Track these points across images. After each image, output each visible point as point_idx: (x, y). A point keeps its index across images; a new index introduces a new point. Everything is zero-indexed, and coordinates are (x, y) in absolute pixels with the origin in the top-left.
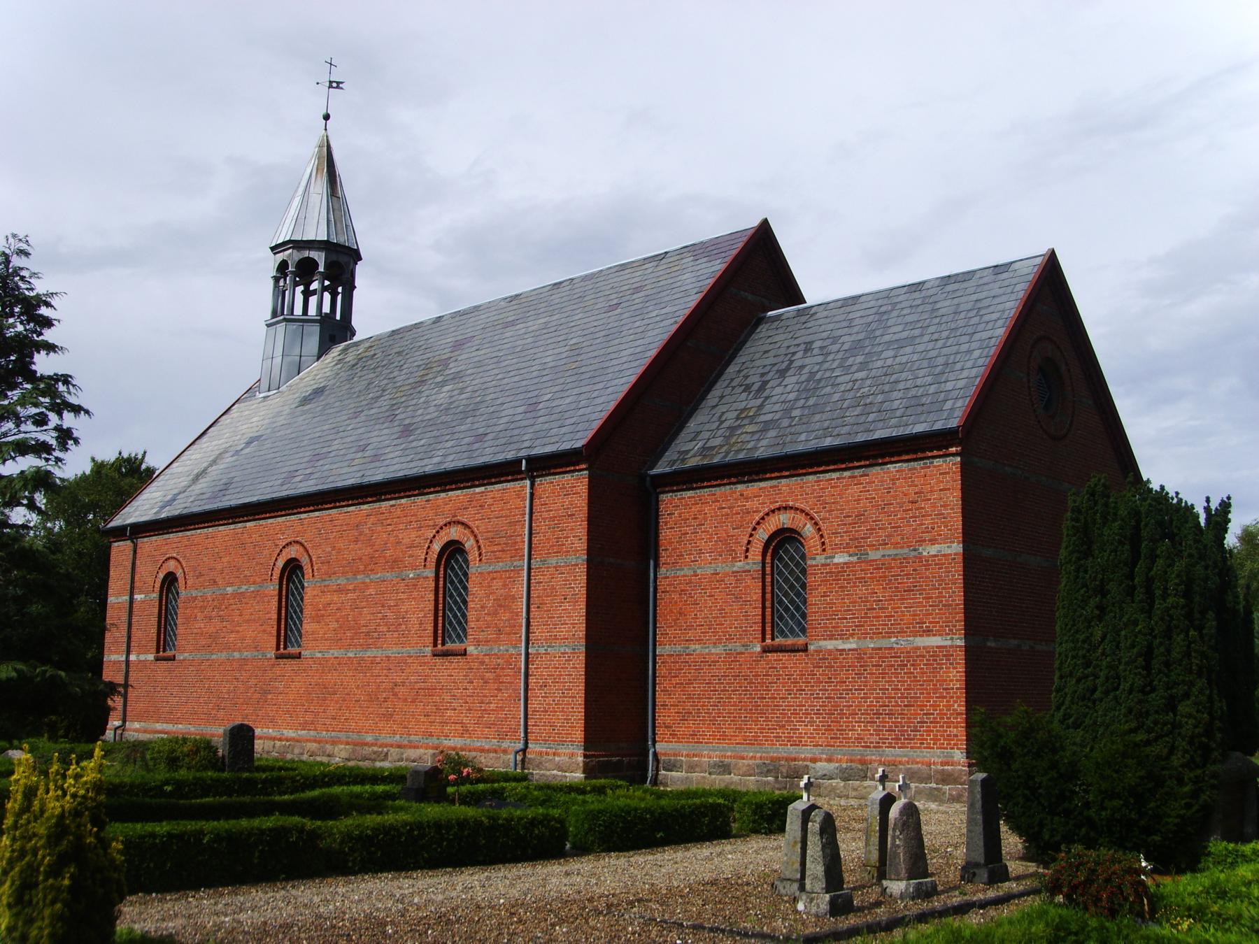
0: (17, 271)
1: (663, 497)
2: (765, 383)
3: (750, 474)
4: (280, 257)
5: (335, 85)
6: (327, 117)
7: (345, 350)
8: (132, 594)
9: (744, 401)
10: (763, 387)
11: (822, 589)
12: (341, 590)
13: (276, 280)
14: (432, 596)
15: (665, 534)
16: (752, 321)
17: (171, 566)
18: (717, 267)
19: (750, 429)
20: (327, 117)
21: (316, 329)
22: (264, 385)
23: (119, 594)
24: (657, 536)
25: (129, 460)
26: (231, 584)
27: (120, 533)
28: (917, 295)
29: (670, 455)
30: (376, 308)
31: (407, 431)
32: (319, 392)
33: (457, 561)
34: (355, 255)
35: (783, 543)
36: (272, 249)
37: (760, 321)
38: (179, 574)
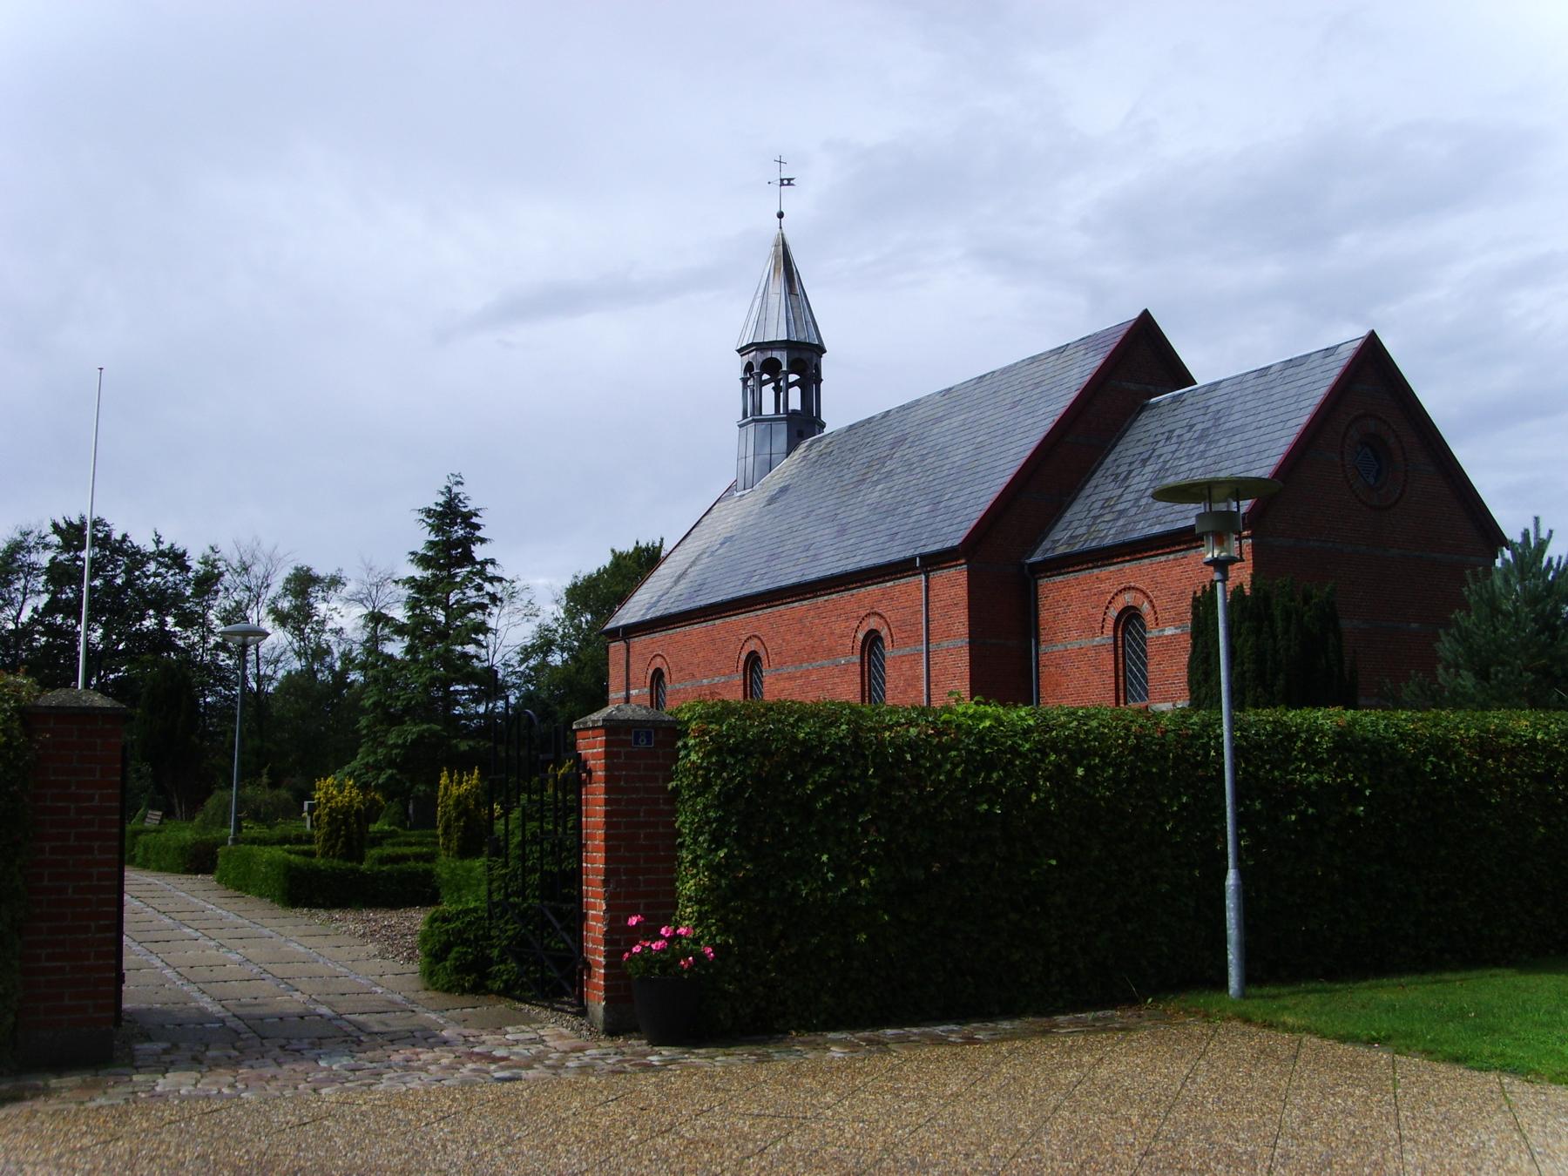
0: (457, 495)
1: (1040, 582)
2: (1130, 472)
3: (1102, 559)
4: (746, 359)
5: (787, 182)
6: (781, 215)
7: (811, 445)
8: (628, 690)
9: (1111, 490)
10: (1126, 478)
11: (1157, 659)
12: (791, 678)
13: (745, 381)
14: (859, 680)
15: (1044, 615)
16: (1136, 407)
17: (658, 662)
18: (1095, 361)
19: (1107, 518)
20: (781, 215)
21: (783, 427)
22: (740, 485)
23: (618, 690)
24: (1037, 616)
25: (647, 549)
26: (706, 677)
27: (614, 634)
28: (1262, 380)
29: (1046, 544)
30: (844, 400)
31: (842, 531)
32: (784, 490)
33: (1134, 626)
34: (820, 350)
35: (1129, 619)
36: (739, 351)
37: (1144, 408)
38: (665, 670)
